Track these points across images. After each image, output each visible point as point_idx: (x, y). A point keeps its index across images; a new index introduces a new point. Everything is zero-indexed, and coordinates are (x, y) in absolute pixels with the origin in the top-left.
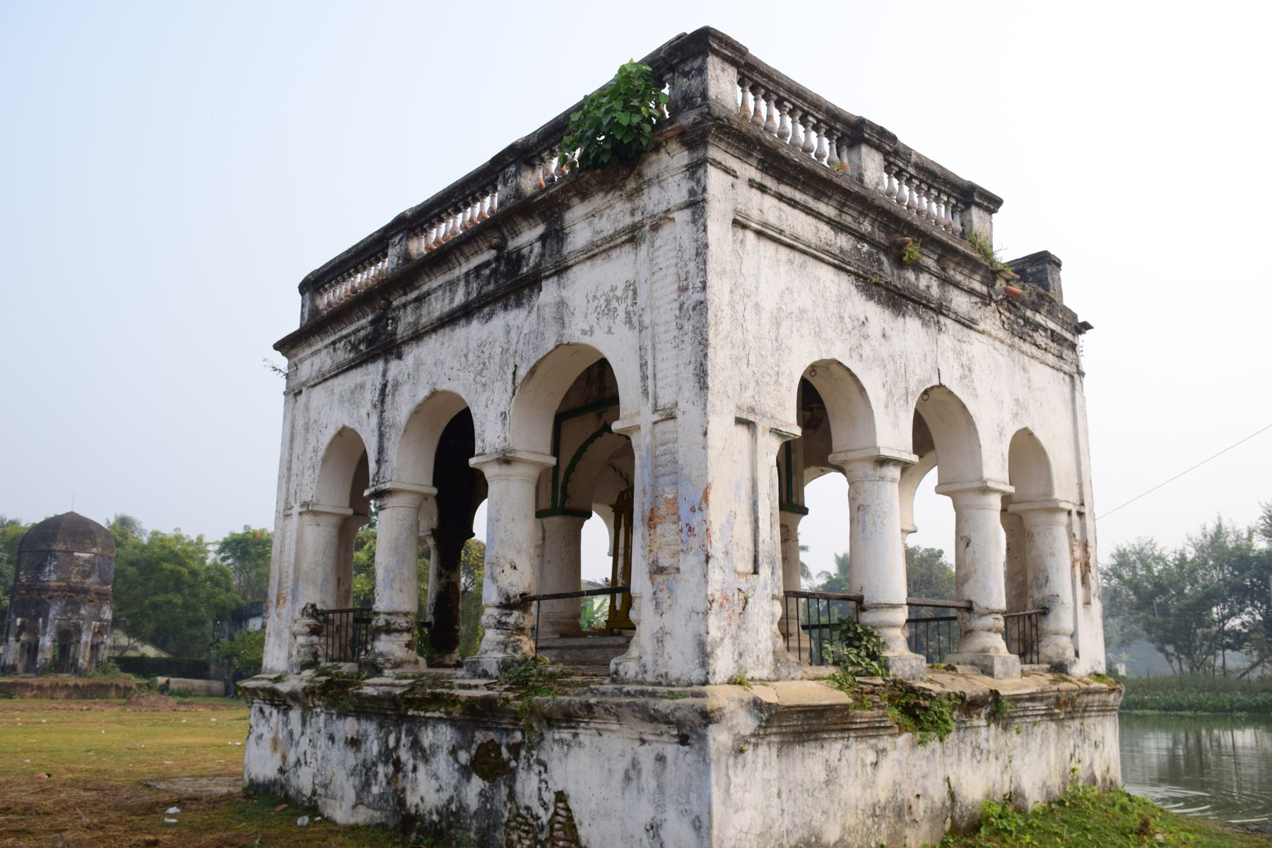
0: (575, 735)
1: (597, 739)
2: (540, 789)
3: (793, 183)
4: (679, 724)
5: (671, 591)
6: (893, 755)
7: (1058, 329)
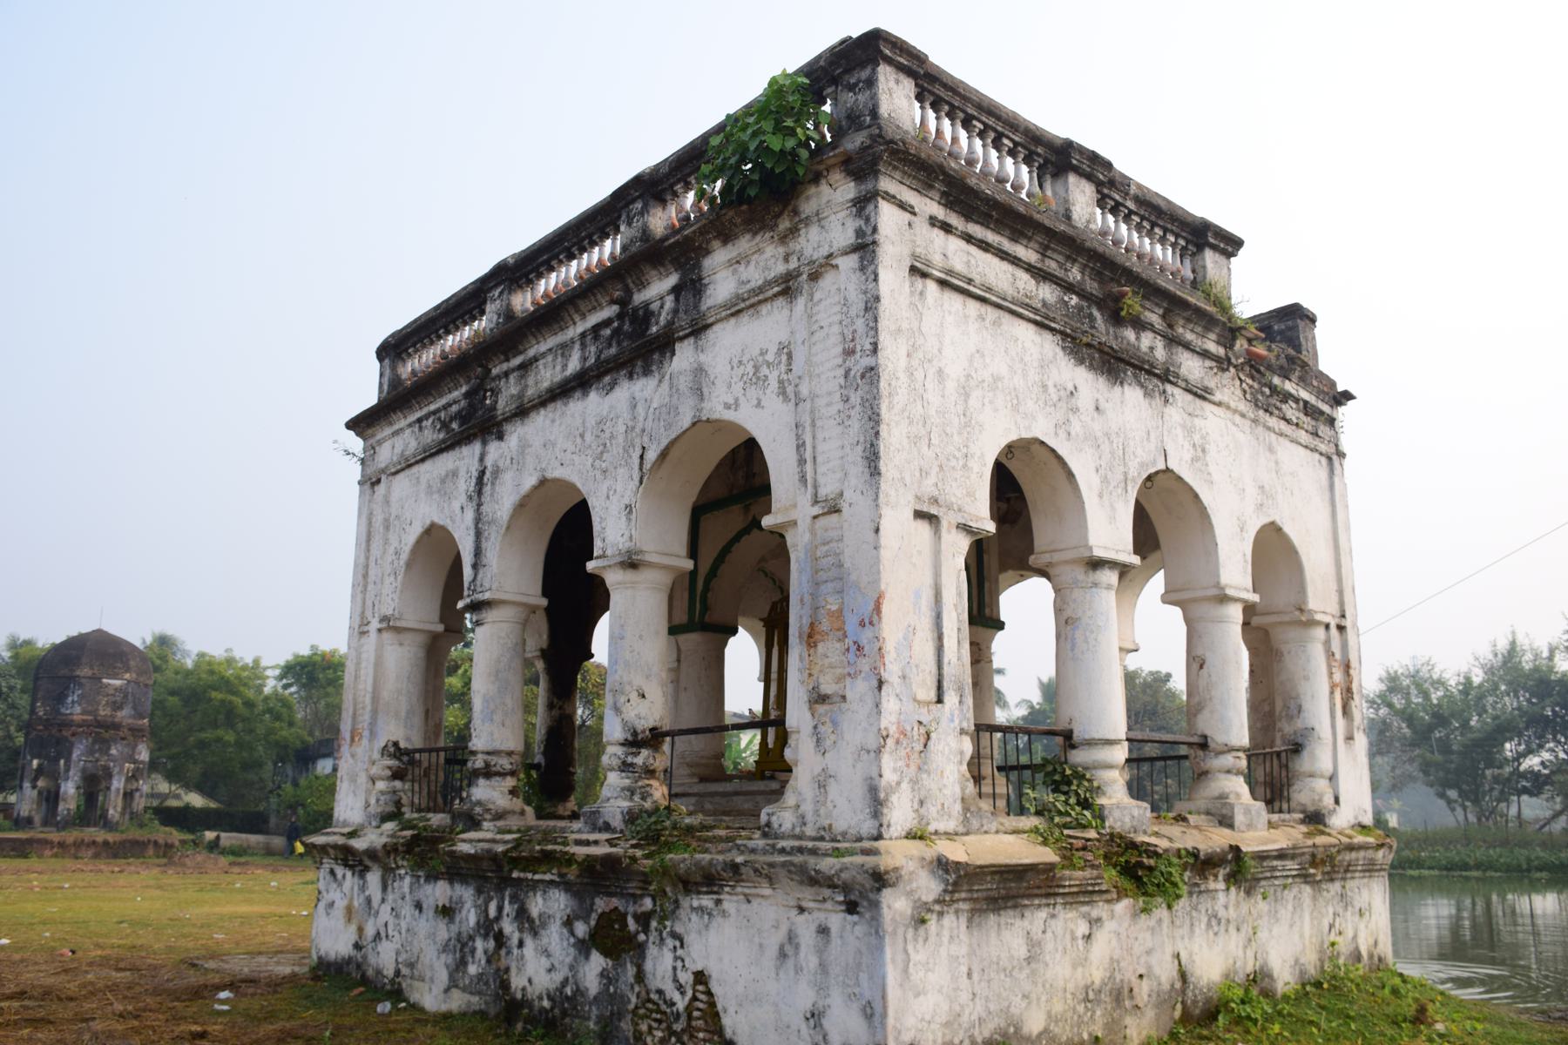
0: (718, 902)
1: (744, 906)
2: (675, 969)
3: (985, 220)
4: (846, 888)
5: (835, 723)
6: (1109, 926)
7: (1312, 399)
